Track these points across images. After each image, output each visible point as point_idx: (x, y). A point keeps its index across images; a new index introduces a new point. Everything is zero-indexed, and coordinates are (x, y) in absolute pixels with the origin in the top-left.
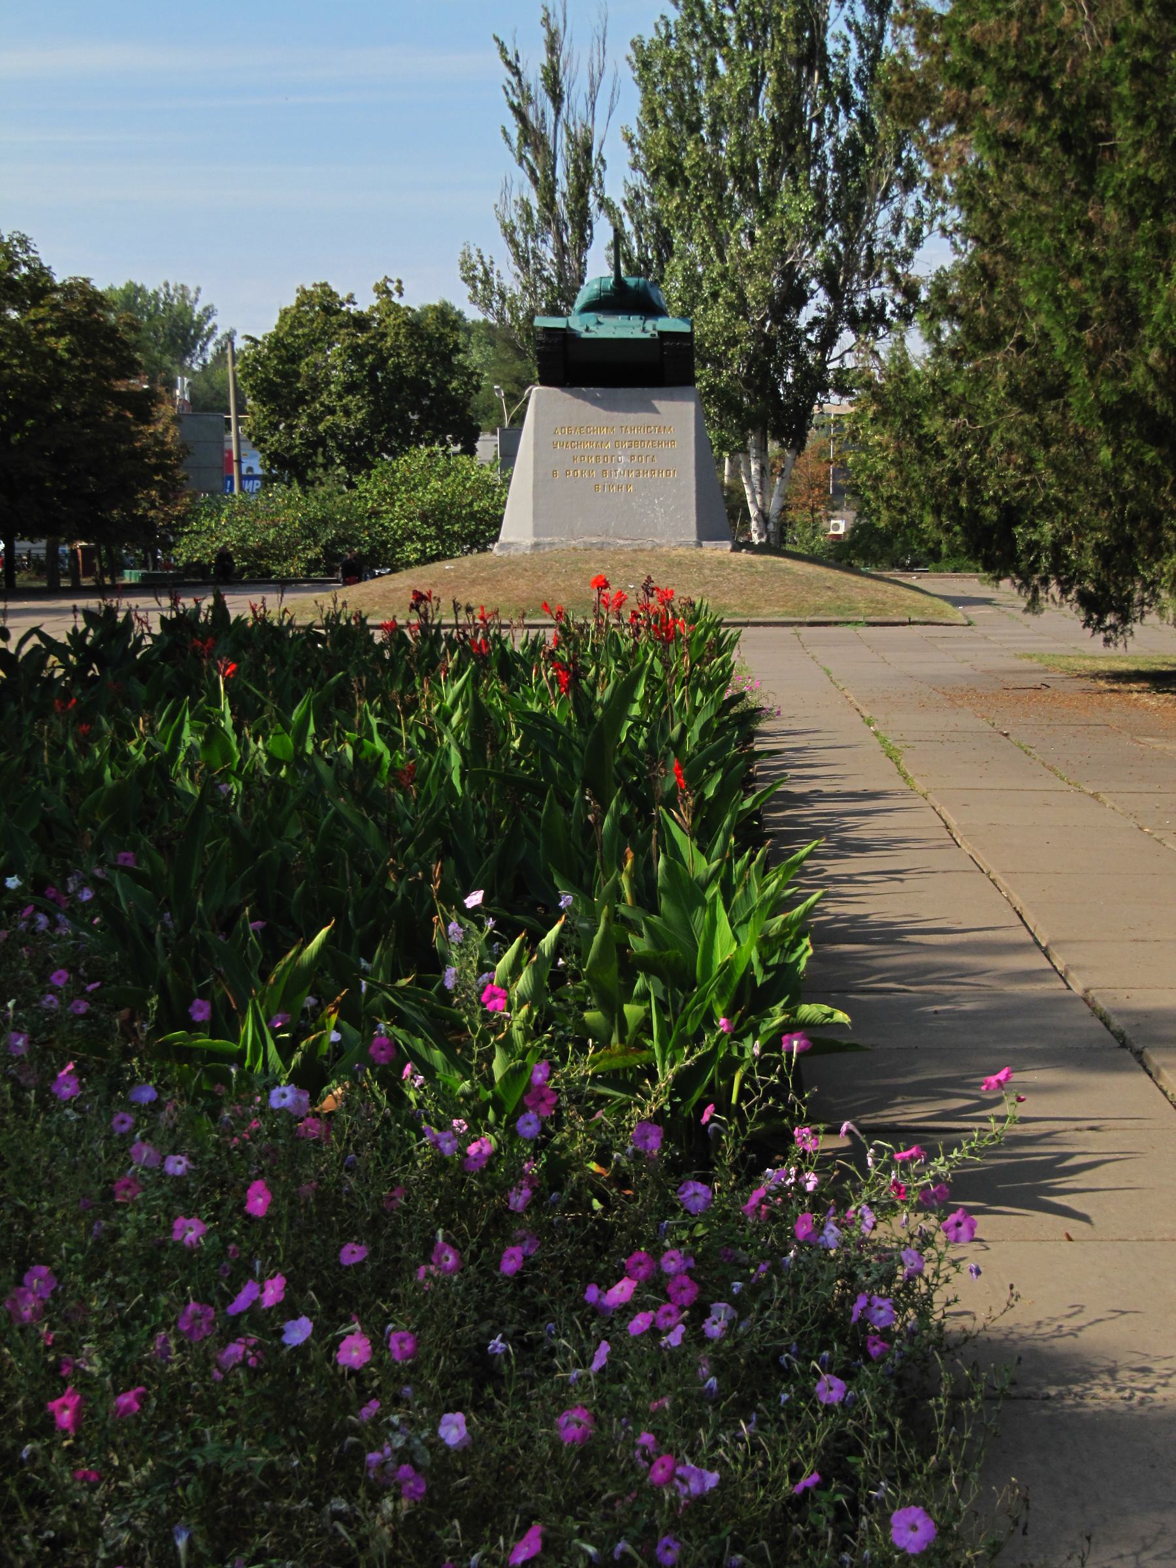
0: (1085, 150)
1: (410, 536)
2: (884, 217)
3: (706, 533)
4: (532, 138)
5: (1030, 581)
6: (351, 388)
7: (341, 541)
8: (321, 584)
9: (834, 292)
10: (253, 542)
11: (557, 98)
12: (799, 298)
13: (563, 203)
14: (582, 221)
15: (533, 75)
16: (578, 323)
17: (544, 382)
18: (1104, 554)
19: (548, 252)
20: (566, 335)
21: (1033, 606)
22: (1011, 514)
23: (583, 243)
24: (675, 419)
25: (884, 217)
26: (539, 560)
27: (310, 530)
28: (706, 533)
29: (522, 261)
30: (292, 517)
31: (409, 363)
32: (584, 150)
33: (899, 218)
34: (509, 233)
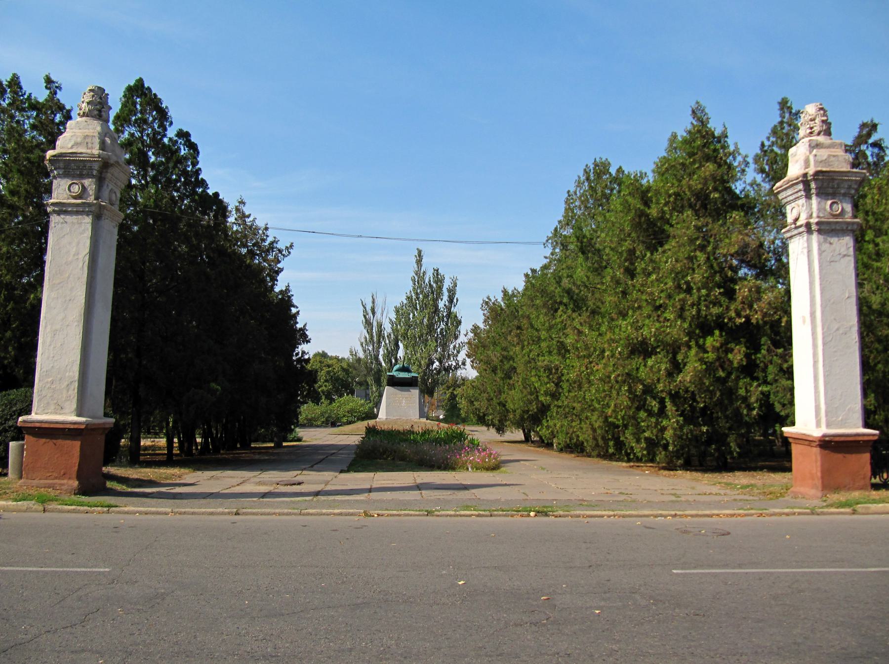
0: (494, 370)
1: (344, 416)
2: (452, 346)
3: (421, 417)
4: (368, 324)
5: (488, 426)
6: (326, 381)
7: (329, 417)
8: (325, 427)
9: (441, 362)
10: (309, 417)
11: (374, 313)
12: (433, 363)
13: (374, 335)
14: (379, 342)
15: (369, 308)
16: (394, 373)
17: (388, 385)
18: (499, 421)
19: (371, 348)
20: (393, 376)
21: (505, 292)
22: (484, 415)
23: (379, 347)
24: (415, 392)
25: (452, 346)
26: (383, 423)
27: (322, 414)
28: (421, 417)
29: (365, 351)
30: (318, 412)
31: (341, 374)
32: (380, 325)
33: (455, 347)
34: (362, 344)
